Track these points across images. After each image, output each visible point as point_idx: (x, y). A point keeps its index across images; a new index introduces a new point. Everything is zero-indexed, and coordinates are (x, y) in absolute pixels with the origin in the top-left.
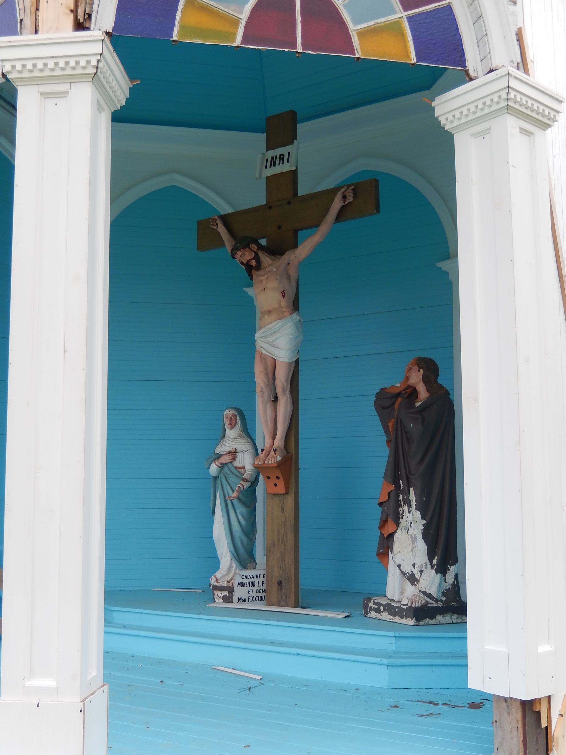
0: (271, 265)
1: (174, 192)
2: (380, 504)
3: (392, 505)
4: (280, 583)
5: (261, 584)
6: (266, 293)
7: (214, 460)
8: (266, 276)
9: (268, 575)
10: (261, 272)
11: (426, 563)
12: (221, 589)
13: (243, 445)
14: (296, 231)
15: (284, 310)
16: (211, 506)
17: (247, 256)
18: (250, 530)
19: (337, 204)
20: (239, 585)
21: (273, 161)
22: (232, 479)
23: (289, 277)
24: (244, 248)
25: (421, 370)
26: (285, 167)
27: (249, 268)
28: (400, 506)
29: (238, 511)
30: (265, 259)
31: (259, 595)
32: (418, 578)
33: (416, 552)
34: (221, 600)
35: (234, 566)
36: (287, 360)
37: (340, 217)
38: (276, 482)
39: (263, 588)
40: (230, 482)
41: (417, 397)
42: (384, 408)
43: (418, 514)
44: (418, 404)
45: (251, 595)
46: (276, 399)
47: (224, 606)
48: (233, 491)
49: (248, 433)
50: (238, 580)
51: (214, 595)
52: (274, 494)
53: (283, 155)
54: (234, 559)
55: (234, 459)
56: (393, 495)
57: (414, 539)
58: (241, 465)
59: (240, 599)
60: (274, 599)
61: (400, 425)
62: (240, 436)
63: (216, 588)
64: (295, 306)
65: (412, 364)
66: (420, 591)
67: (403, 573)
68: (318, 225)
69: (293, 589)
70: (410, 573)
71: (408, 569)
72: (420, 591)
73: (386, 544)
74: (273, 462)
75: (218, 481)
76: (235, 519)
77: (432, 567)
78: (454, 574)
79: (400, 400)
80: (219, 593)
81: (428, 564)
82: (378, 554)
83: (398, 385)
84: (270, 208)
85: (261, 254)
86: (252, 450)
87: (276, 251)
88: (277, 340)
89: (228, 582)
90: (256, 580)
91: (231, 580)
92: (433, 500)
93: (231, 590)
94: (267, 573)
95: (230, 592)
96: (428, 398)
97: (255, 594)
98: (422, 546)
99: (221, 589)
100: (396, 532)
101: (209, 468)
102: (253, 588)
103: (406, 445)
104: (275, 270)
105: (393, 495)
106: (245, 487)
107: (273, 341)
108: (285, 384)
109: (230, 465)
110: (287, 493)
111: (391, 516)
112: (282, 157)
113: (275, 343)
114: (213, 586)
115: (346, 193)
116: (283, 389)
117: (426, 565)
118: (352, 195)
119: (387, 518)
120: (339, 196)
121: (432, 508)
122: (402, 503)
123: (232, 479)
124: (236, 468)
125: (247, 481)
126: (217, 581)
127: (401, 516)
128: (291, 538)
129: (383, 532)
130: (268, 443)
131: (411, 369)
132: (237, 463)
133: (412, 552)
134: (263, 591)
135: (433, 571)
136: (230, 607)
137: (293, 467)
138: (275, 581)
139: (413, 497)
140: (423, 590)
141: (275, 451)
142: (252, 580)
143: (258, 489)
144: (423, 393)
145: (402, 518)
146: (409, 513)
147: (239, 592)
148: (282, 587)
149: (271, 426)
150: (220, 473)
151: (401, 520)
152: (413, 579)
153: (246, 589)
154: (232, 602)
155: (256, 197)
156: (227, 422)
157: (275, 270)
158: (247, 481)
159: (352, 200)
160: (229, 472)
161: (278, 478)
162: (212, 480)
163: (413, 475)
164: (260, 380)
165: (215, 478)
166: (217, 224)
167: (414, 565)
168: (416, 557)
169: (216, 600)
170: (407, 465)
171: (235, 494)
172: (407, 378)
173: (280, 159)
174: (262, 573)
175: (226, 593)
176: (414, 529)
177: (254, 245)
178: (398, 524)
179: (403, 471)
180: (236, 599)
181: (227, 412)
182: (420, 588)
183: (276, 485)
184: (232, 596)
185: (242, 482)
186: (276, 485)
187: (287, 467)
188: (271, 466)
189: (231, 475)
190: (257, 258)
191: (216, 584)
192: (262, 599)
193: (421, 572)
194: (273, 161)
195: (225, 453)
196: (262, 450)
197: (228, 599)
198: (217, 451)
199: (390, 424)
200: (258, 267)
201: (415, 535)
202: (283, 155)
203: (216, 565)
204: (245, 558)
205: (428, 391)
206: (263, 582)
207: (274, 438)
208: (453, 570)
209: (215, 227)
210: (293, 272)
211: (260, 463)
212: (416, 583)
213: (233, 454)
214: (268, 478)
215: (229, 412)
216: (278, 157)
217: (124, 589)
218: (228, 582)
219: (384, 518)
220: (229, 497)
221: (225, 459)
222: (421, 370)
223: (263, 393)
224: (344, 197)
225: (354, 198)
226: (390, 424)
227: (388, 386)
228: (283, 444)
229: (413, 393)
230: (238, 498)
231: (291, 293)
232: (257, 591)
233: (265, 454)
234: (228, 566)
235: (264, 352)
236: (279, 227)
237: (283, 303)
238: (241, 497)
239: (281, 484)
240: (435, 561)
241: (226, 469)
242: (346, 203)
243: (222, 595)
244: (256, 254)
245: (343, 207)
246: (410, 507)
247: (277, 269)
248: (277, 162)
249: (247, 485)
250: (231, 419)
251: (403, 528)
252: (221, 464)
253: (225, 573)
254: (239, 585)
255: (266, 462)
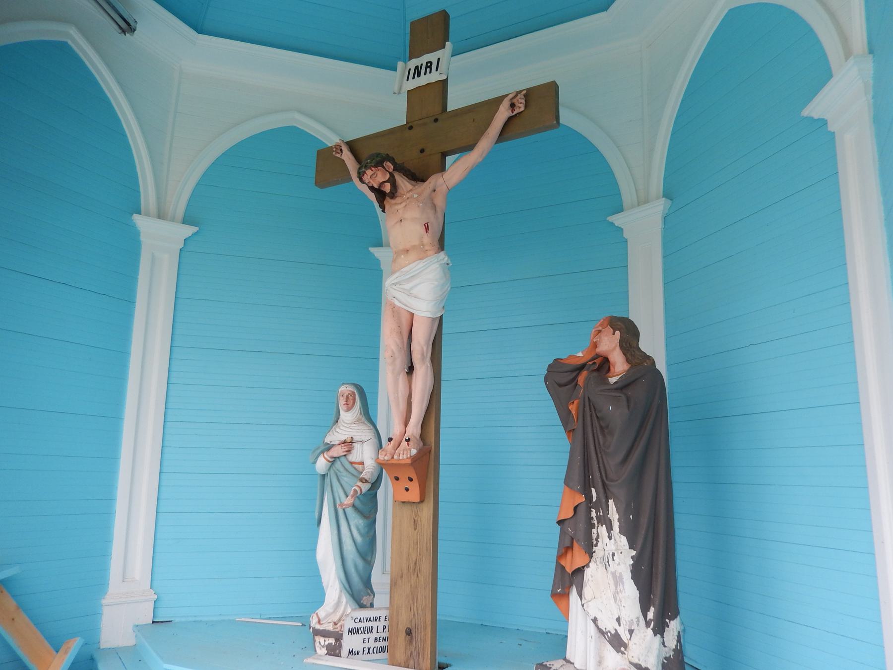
0: (411, 190)
1: (293, 132)
2: (560, 522)
3: (582, 526)
4: (409, 632)
5: (380, 629)
6: (405, 222)
7: (323, 452)
8: (404, 204)
9: (391, 627)
10: (398, 200)
11: (638, 618)
12: (325, 634)
13: (362, 433)
14: (444, 155)
15: (426, 248)
16: (317, 514)
17: (378, 177)
18: (367, 552)
19: (503, 114)
20: (351, 631)
21: (418, 71)
22: (346, 479)
23: (434, 207)
24: (376, 166)
25: (618, 332)
26: (433, 77)
27: (381, 195)
28: (593, 526)
29: (352, 523)
30: (403, 183)
31: (378, 644)
32: (626, 641)
33: (623, 600)
34: (324, 651)
35: (344, 600)
36: (429, 315)
37: (503, 135)
38: (408, 485)
39: (385, 635)
40: (343, 483)
41: (609, 370)
42: (560, 385)
43: (623, 541)
44: (612, 380)
45: (367, 645)
46: (411, 369)
47: (328, 664)
48: (347, 496)
49: (368, 416)
50: (350, 624)
51: (315, 641)
52: (403, 502)
53: (431, 63)
54: (344, 591)
55: (349, 451)
56: (582, 511)
57: (618, 580)
58: (358, 460)
59: (351, 652)
60: (400, 655)
61: (590, 407)
62: (358, 421)
63: (317, 633)
64: (441, 245)
65: (601, 325)
66: (631, 663)
67: (602, 632)
68: (470, 147)
69: (429, 643)
70: (613, 632)
71: (609, 625)
72: (631, 663)
73: (568, 580)
74: (405, 457)
75: (327, 480)
76: (348, 534)
77: (648, 624)
78: (676, 634)
79: (584, 373)
80: (322, 640)
81: (642, 618)
82: (554, 595)
83: (580, 354)
84: (411, 128)
85: (399, 178)
86: (375, 440)
87: (417, 177)
88: (415, 286)
89: (335, 624)
90: (374, 624)
91: (339, 620)
92: (644, 520)
93: (338, 637)
94: (391, 615)
95: (336, 640)
96: (628, 370)
97: (372, 644)
98: (631, 592)
99: (325, 634)
100: (587, 565)
101: (315, 462)
102: (369, 635)
103: (600, 437)
104: (416, 196)
105: (582, 511)
106: (364, 491)
107: (411, 288)
108: (425, 349)
109: (343, 459)
110: (422, 501)
111: (576, 536)
112: (429, 65)
113: (414, 292)
114: (314, 629)
115: (515, 101)
116: (423, 355)
117: (638, 621)
118: (523, 101)
119: (572, 543)
120: (506, 104)
121: (643, 532)
122: (595, 522)
123: (345, 479)
124: (352, 463)
125: (366, 481)
126: (319, 622)
127: (595, 542)
128: (426, 567)
129: (563, 563)
130: (396, 429)
131: (600, 331)
132: (354, 457)
133: (615, 599)
134: (384, 639)
135: (650, 631)
136: (336, 665)
137: (432, 463)
138: (402, 629)
139: (614, 514)
140: (635, 661)
141: (408, 440)
142: (369, 624)
143: (380, 493)
144: (620, 365)
145: (596, 545)
146: (610, 538)
147: (350, 642)
148: (411, 638)
149: (403, 406)
150: (329, 469)
151: (595, 549)
152: (617, 643)
153: (359, 637)
154: (339, 655)
155: (396, 114)
156: (342, 402)
157: (416, 196)
158: (366, 481)
159: (522, 109)
160: (342, 469)
161: (411, 480)
162: (319, 478)
163: (612, 481)
164: (389, 341)
165: (324, 476)
166: (341, 150)
167: (618, 620)
168: (622, 608)
169: (318, 649)
170: (601, 465)
171: (348, 501)
172: (595, 345)
173: (427, 67)
174: (383, 613)
175: (332, 641)
176: (619, 564)
177: (389, 164)
178: (590, 552)
179: (597, 474)
180: (345, 652)
181: (343, 389)
182: (630, 658)
183: (407, 490)
184: (340, 646)
185: (360, 484)
186: (407, 490)
187: (424, 466)
188: (403, 462)
189: (345, 473)
190: (392, 181)
191: (318, 627)
192: (382, 650)
193: (631, 632)
194: (418, 71)
195: (337, 443)
196: (390, 440)
197: (334, 651)
198: (327, 440)
199: (573, 408)
200: (393, 194)
201: (620, 573)
202: (431, 63)
203: (320, 601)
204: (360, 592)
205: (628, 360)
206: (384, 627)
207: (406, 424)
208: (674, 626)
209: (338, 155)
210: (439, 201)
211: (386, 458)
212: (623, 649)
213: (349, 444)
214: (397, 479)
215: (345, 389)
216: (424, 66)
217: (199, 619)
218: (335, 624)
219: (568, 543)
220: (341, 504)
221: (338, 451)
222: (618, 332)
223: (394, 360)
224: (513, 106)
225: (526, 107)
226: (573, 408)
227: (563, 356)
228: (419, 431)
229: (603, 365)
230: (354, 506)
231: (435, 228)
232: (376, 639)
233: (394, 445)
234: (335, 601)
235: (397, 303)
236: (422, 151)
237: (427, 239)
238: (358, 503)
239: (415, 487)
240: (651, 615)
241: (338, 465)
242: (515, 113)
243: (326, 643)
244: (392, 175)
245: (510, 119)
246: (610, 529)
247: (420, 195)
248: (423, 71)
249: (365, 487)
250: (347, 397)
251: (598, 561)
252: (332, 457)
253: (332, 611)
254: (351, 631)
255: (395, 457)
